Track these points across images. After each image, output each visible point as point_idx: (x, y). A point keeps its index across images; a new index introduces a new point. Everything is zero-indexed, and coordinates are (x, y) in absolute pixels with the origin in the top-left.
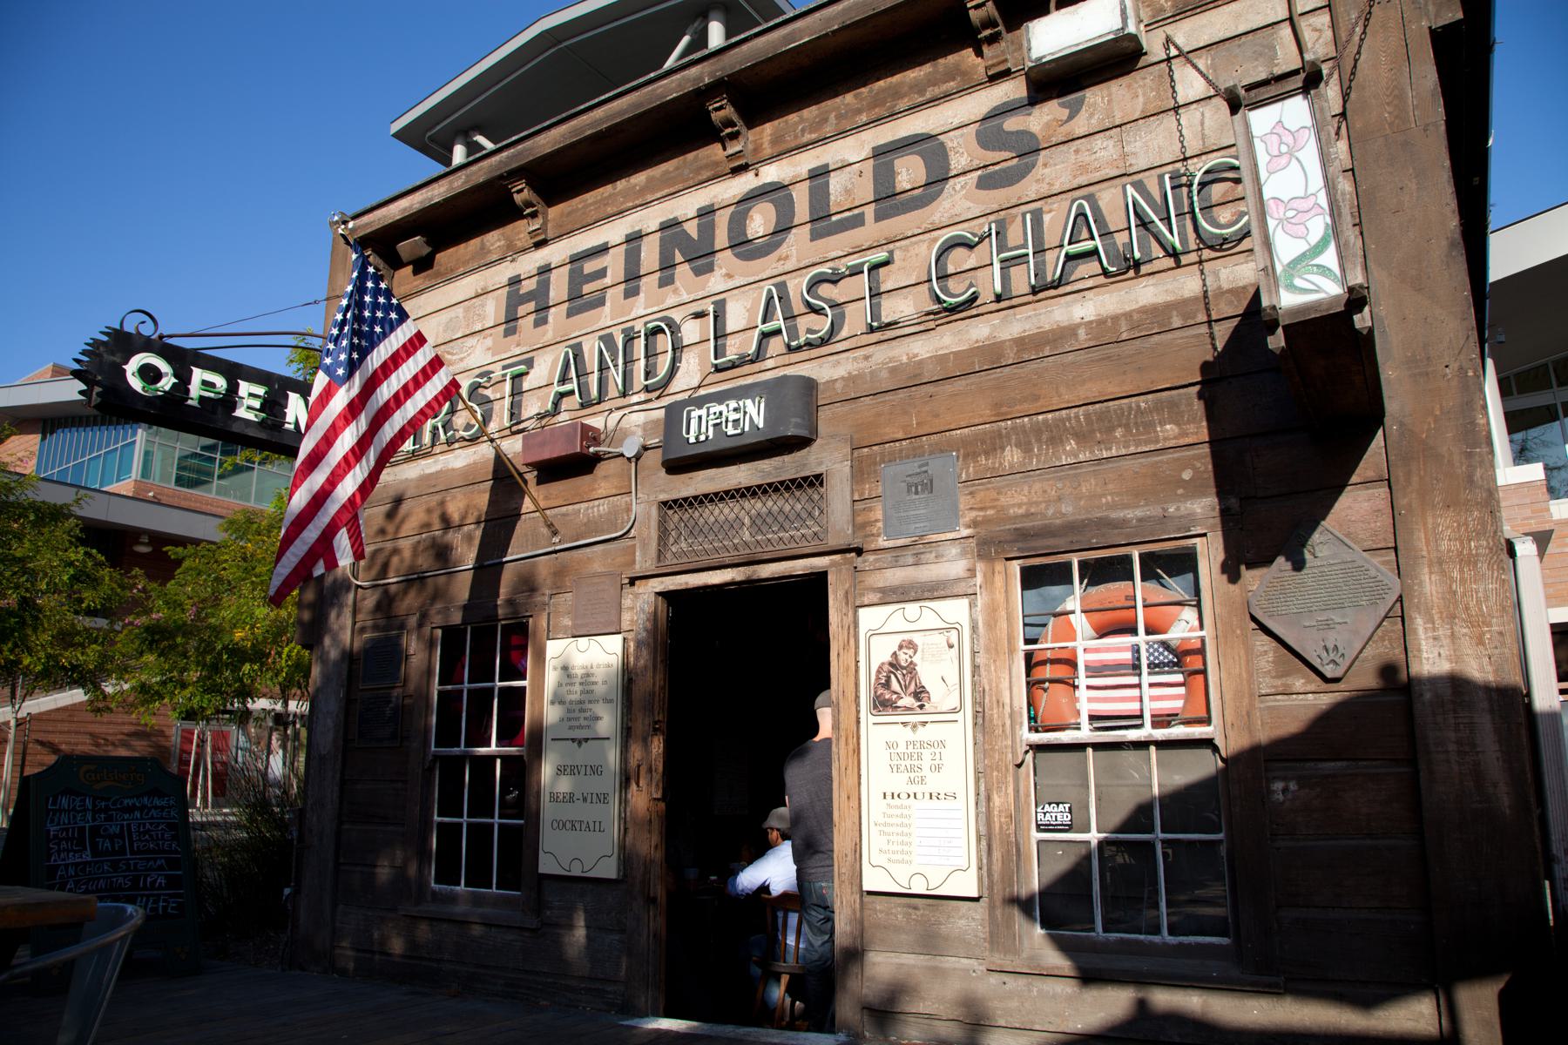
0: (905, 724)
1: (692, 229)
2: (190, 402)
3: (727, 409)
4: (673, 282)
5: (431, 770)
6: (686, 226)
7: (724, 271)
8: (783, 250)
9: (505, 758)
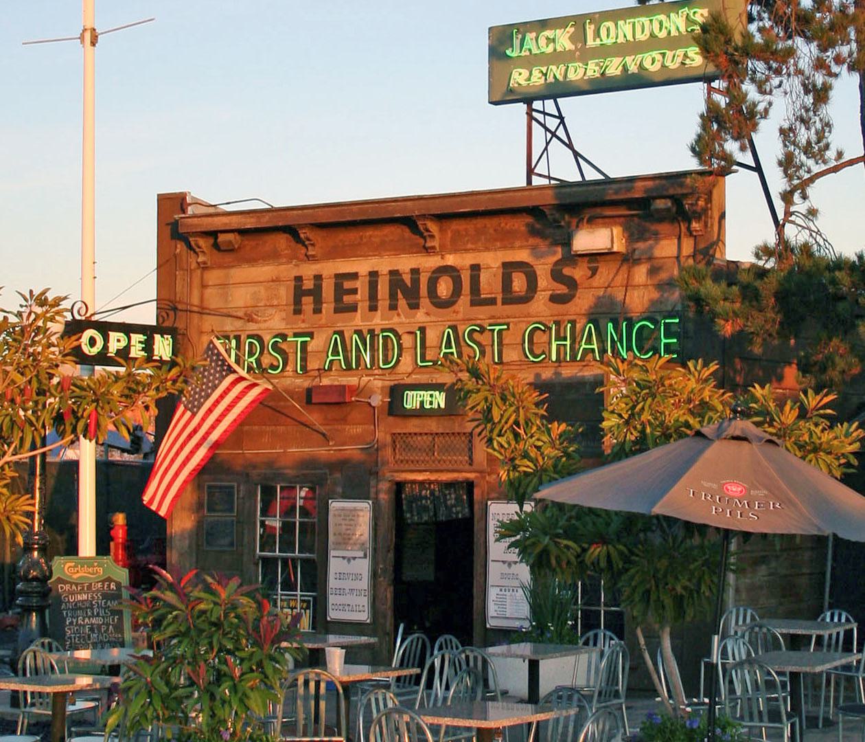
0: (344, 558)
1: (407, 278)
2: (109, 355)
3: (425, 395)
4: (396, 309)
5: (257, 564)
6: (404, 277)
7: (425, 310)
8: (456, 307)
9: (304, 561)
